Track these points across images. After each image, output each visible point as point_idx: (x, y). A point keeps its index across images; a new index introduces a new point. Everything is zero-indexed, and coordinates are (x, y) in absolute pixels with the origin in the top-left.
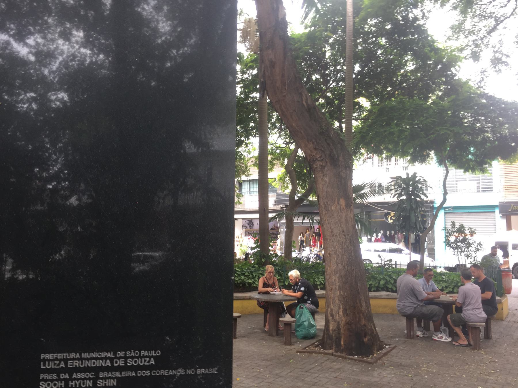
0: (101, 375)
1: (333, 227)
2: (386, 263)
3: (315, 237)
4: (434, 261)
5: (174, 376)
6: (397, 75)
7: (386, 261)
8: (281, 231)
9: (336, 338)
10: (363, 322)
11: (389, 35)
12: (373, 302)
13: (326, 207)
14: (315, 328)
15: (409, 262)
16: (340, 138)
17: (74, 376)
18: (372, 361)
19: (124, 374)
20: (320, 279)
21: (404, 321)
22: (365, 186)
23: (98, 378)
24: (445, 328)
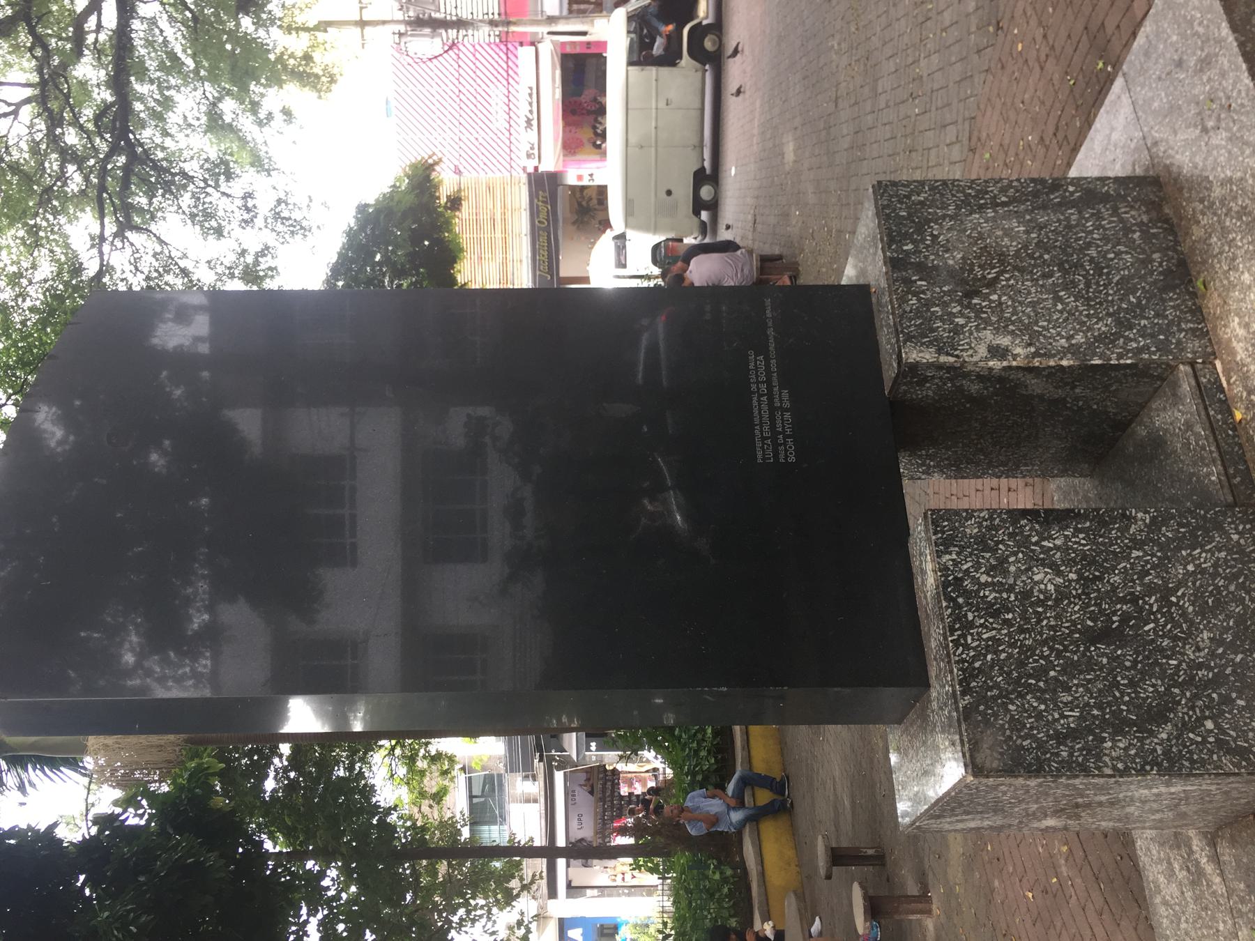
19: (775, 382)
23: (781, 407)
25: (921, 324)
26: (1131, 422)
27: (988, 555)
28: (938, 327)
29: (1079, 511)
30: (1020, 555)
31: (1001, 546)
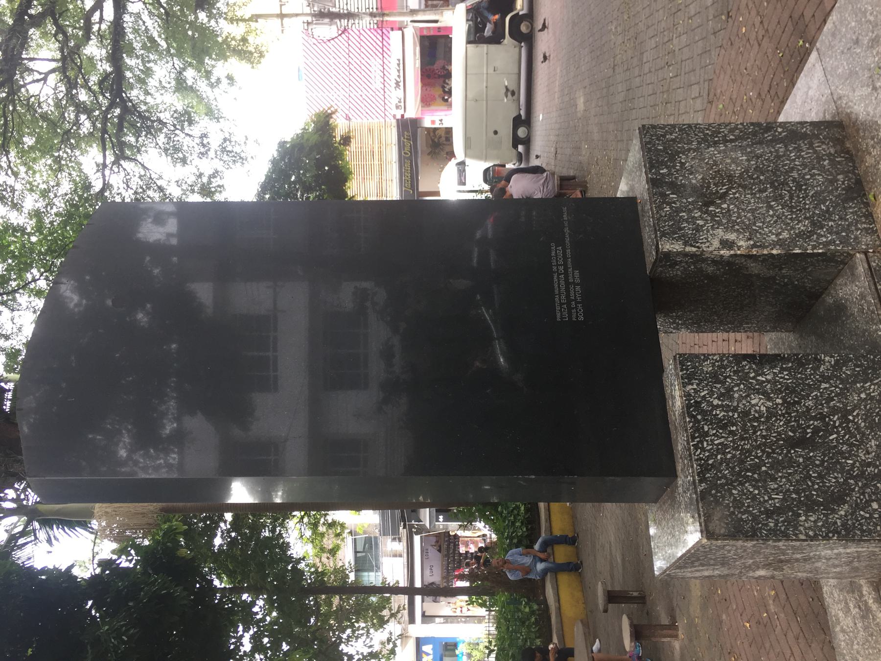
0: (571, 280)
8: (443, 529)
19: (570, 265)
23: (573, 282)
26: (822, 293)
27: (719, 386)
28: (685, 227)
29: (784, 355)
30: (742, 386)
31: (728, 380)
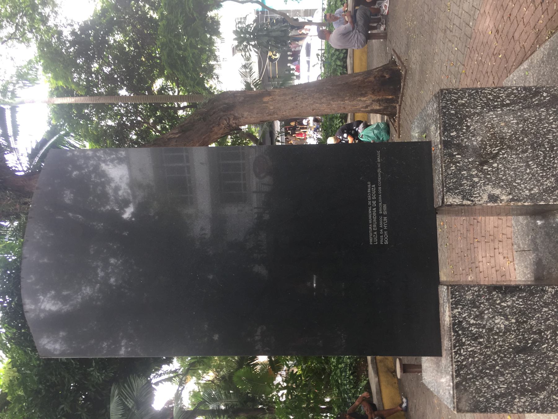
1: (289, 108)
2: (320, 60)
3: (296, 134)
4: (317, 11)
5: (381, 174)
6: (129, 51)
7: (319, 59)
9: (387, 102)
10: (372, 79)
11: (89, 60)
12: (357, 70)
13: (271, 114)
14: (379, 124)
15: (317, 37)
16: (208, 102)
17: (381, 226)
18: (404, 70)
20: (337, 123)
21: (375, 42)
22: (246, 82)
24: (377, 4)
25: (456, 181)
28: (465, 183)
